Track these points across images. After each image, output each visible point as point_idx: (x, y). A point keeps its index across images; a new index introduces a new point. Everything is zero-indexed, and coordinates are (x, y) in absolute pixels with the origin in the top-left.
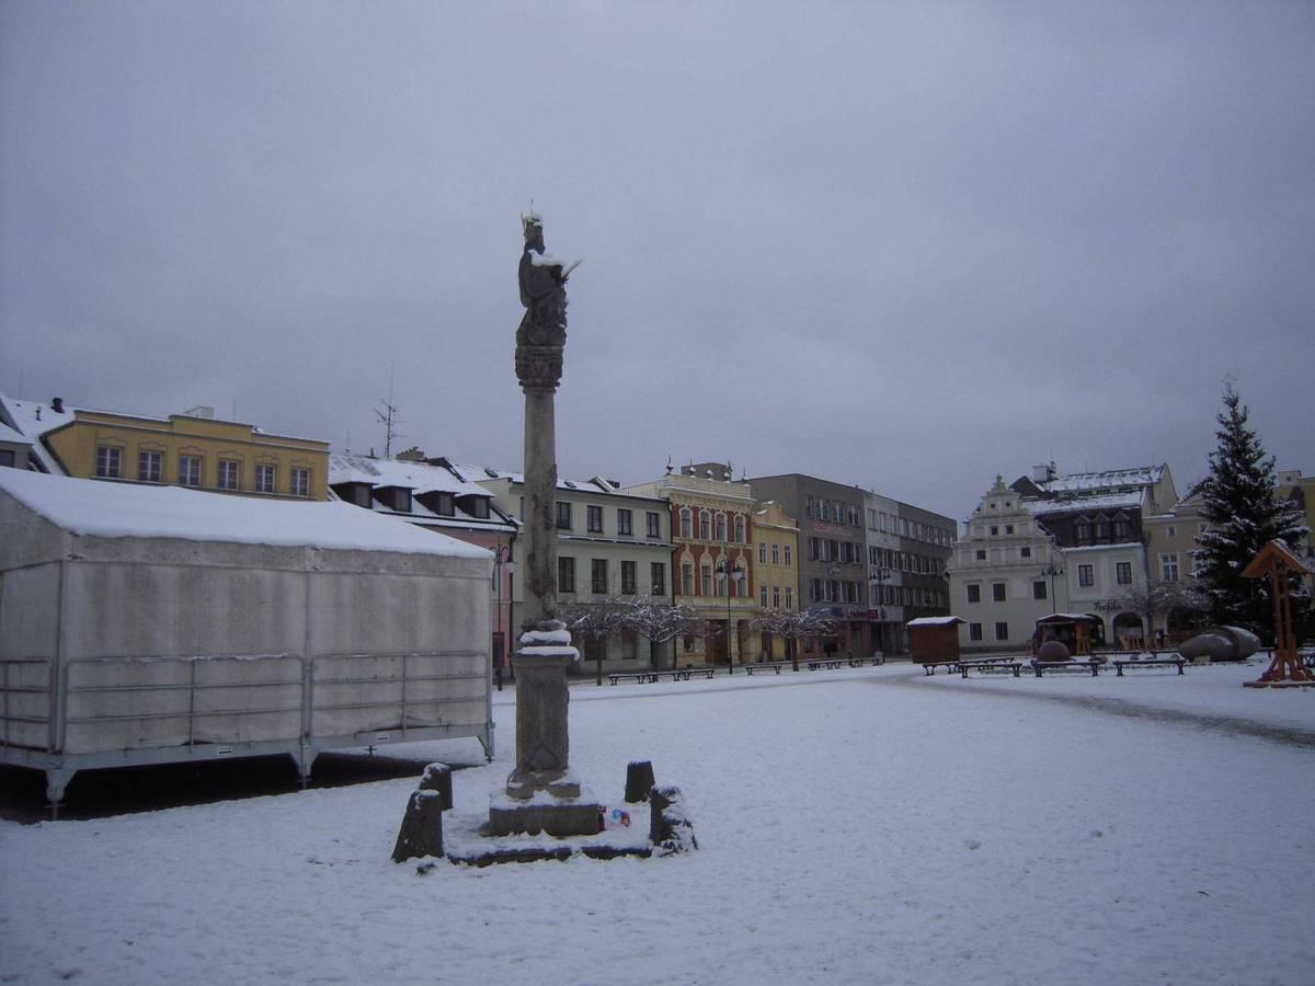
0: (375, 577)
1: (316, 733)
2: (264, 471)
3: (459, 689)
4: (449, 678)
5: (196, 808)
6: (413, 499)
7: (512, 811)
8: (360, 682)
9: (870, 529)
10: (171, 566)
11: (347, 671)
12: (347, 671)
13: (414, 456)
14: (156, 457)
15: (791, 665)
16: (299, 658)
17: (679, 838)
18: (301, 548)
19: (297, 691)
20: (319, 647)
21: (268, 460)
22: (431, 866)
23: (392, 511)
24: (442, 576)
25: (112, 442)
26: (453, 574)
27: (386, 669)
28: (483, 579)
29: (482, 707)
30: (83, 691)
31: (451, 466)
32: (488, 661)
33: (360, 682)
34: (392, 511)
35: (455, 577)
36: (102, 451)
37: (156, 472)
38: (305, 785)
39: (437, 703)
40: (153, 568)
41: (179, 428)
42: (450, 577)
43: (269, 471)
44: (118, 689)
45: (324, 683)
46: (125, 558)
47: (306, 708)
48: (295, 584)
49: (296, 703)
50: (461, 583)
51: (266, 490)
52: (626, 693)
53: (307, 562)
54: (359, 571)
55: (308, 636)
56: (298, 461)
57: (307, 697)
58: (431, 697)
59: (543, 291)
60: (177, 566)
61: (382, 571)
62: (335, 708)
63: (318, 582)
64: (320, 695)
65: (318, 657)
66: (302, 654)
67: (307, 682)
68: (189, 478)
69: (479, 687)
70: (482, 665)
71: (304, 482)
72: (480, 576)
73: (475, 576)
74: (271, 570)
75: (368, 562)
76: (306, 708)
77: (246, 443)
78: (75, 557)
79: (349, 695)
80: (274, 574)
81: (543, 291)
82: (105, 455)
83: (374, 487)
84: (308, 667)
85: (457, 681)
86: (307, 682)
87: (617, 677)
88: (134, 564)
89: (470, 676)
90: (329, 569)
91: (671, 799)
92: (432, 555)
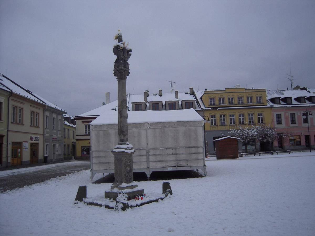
0: (165, 129)
1: (151, 167)
2: (249, 98)
3: (194, 156)
4: (190, 154)
5: (160, 181)
6: (281, 101)
7: (107, 192)
8: (163, 155)
9: (11, 123)
10: (113, 130)
11: (158, 152)
12: (158, 152)
13: (298, 88)
14: (260, 97)
15: (309, 150)
16: (145, 149)
17: (117, 207)
18: (144, 123)
19: (145, 157)
20: (150, 147)
21: (250, 95)
22: (77, 203)
23: (300, 104)
24: (186, 127)
25: (212, 97)
26: (190, 126)
27: (170, 151)
28: (200, 127)
29: (202, 162)
30: (96, 157)
31: (307, 89)
32: (203, 149)
33: (163, 155)
34: (300, 104)
35: (191, 127)
36: (211, 99)
37: (241, 99)
38: (149, 180)
39: (187, 160)
40: (109, 131)
41: (227, 91)
42: (189, 127)
43: (251, 98)
44: (103, 157)
45: (153, 155)
46: (102, 129)
47: (148, 161)
48: (143, 132)
49: (145, 160)
50: (193, 128)
51: (251, 103)
52: (257, 158)
53: (146, 127)
54: (160, 127)
55: (147, 144)
56: (239, 95)
57: (148, 158)
58: (185, 158)
59: (122, 54)
60: (114, 130)
61: (167, 127)
62: (156, 161)
63: (150, 131)
64: (151, 158)
65: (151, 149)
66: (146, 148)
67: (148, 155)
68: (259, 101)
69: (201, 156)
70: (201, 150)
71: (260, 100)
72: (199, 126)
73: (198, 126)
74: (137, 129)
75: (163, 126)
76: (148, 161)
77: (244, 92)
78: (92, 130)
79: (159, 158)
80: (137, 130)
81: (122, 54)
82: (211, 100)
83: (306, 97)
84: (148, 152)
85: (194, 155)
86: (148, 155)
87: (278, 152)
88: (105, 130)
89: (198, 153)
90: (152, 128)
91: (119, 195)
92: (183, 122)
